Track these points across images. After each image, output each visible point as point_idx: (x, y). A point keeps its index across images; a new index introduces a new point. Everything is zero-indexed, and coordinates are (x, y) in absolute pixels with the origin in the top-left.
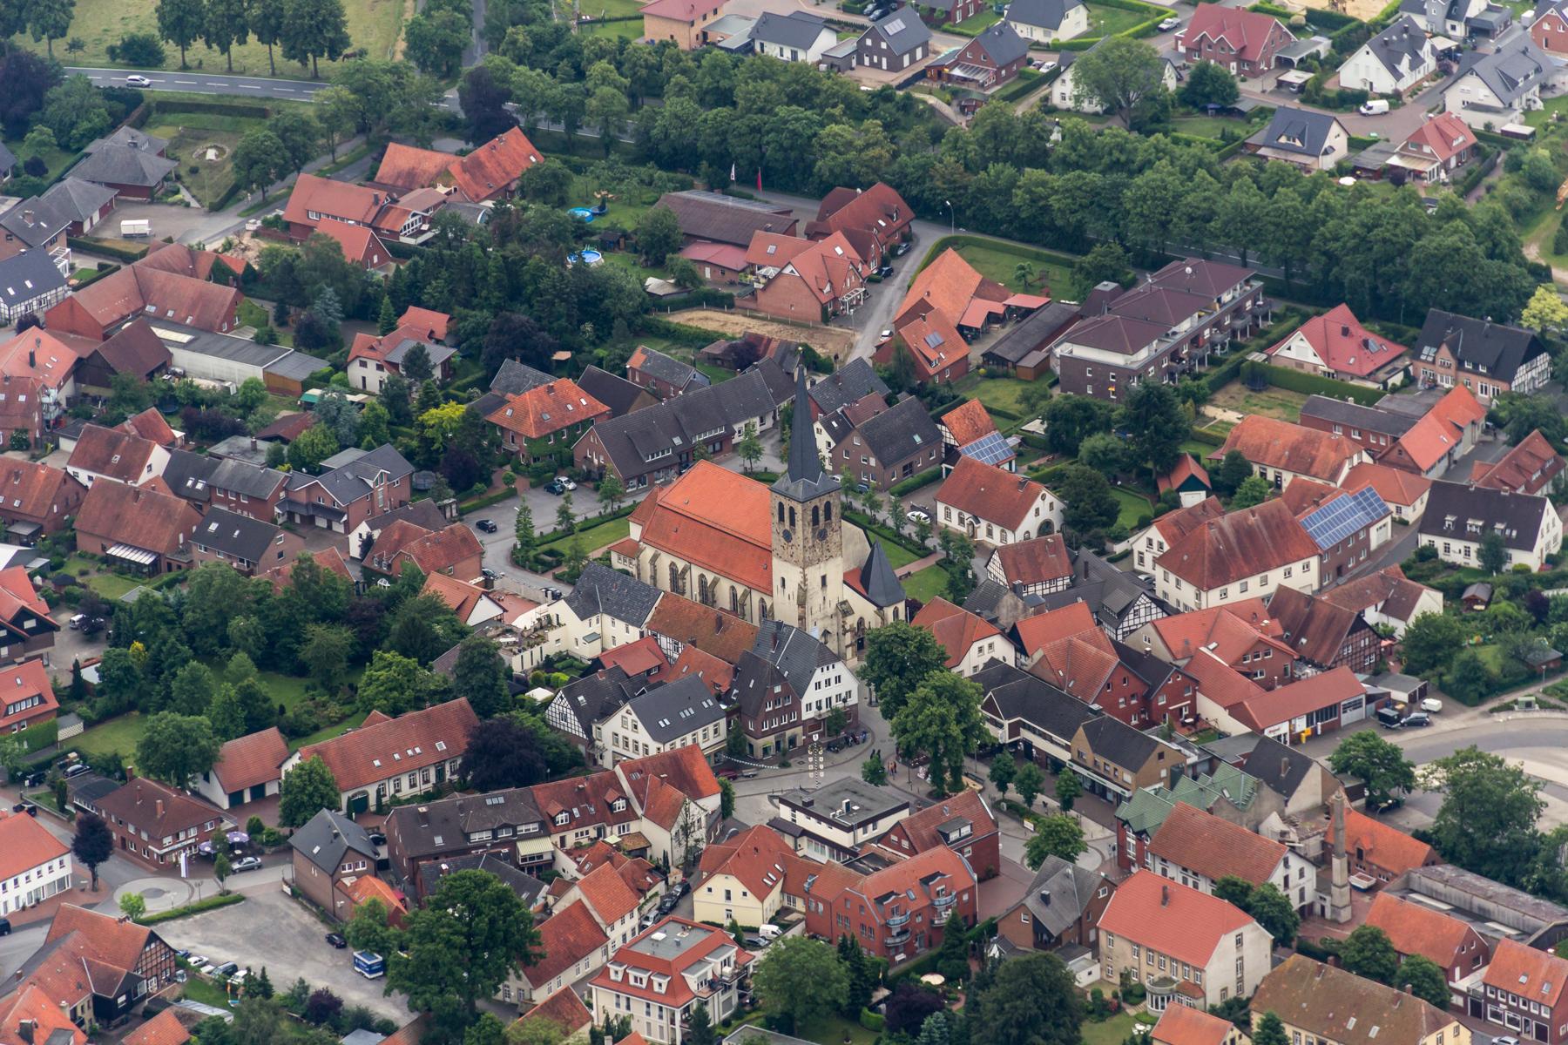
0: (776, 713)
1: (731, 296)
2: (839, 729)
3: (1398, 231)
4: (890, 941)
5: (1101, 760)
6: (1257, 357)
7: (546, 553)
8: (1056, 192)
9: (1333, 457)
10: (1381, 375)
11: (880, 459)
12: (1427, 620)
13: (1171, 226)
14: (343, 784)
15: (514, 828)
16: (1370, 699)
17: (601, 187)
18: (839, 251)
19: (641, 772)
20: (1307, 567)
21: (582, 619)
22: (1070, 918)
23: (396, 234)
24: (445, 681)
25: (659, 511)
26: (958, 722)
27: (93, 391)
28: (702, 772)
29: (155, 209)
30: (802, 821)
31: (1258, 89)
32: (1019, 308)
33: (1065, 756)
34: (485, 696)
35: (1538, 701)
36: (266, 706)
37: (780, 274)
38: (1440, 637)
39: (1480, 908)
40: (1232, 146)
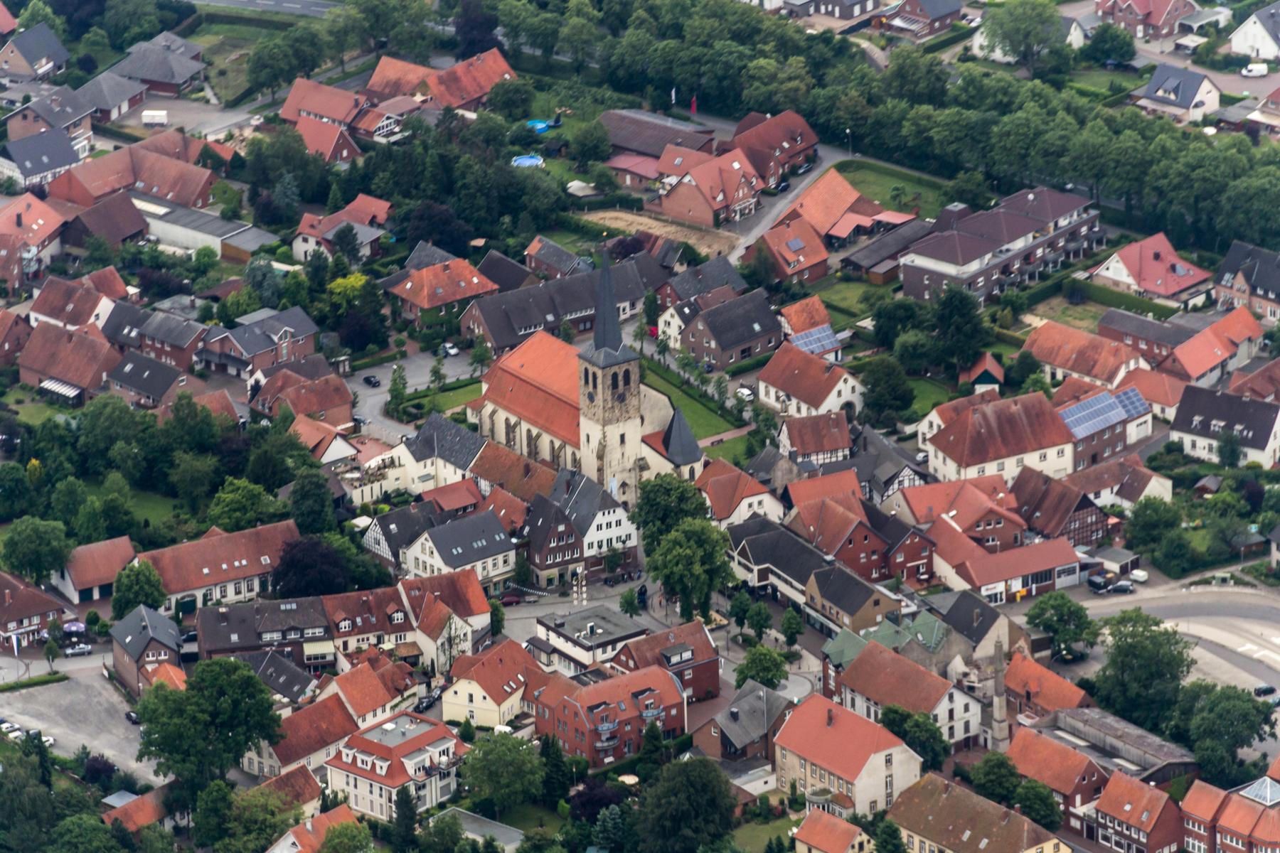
0: (559, 549)
1: (640, 200)
2: (614, 566)
3: (1218, 172)
4: (599, 745)
5: (828, 604)
6: (1081, 275)
7: (414, 406)
8: (938, 126)
9: (1112, 361)
10: (1184, 296)
11: (719, 343)
12: (1151, 504)
13: (1029, 159)
14: (173, 587)
15: (302, 631)
16: (1084, 567)
17: (561, 104)
18: (736, 165)
19: (419, 589)
20: (1061, 453)
21: (418, 460)
22: (756, 734)
23: (371, 134)
24: (285, 506)
25: (500, 373)
26: (703, 563)
27: (75, 251)
28: (475, 595)
29: (180, 104)
30: (557, 641)
31: (1158, 50)
32: (888, 224)
33: (801, 599)
34: (314, 520)
35: (1233, 577)
36: (125, 518)
37: (680, 182)
38: (1155, 518)
39: (1113, 747)
40: (1120, 97)
